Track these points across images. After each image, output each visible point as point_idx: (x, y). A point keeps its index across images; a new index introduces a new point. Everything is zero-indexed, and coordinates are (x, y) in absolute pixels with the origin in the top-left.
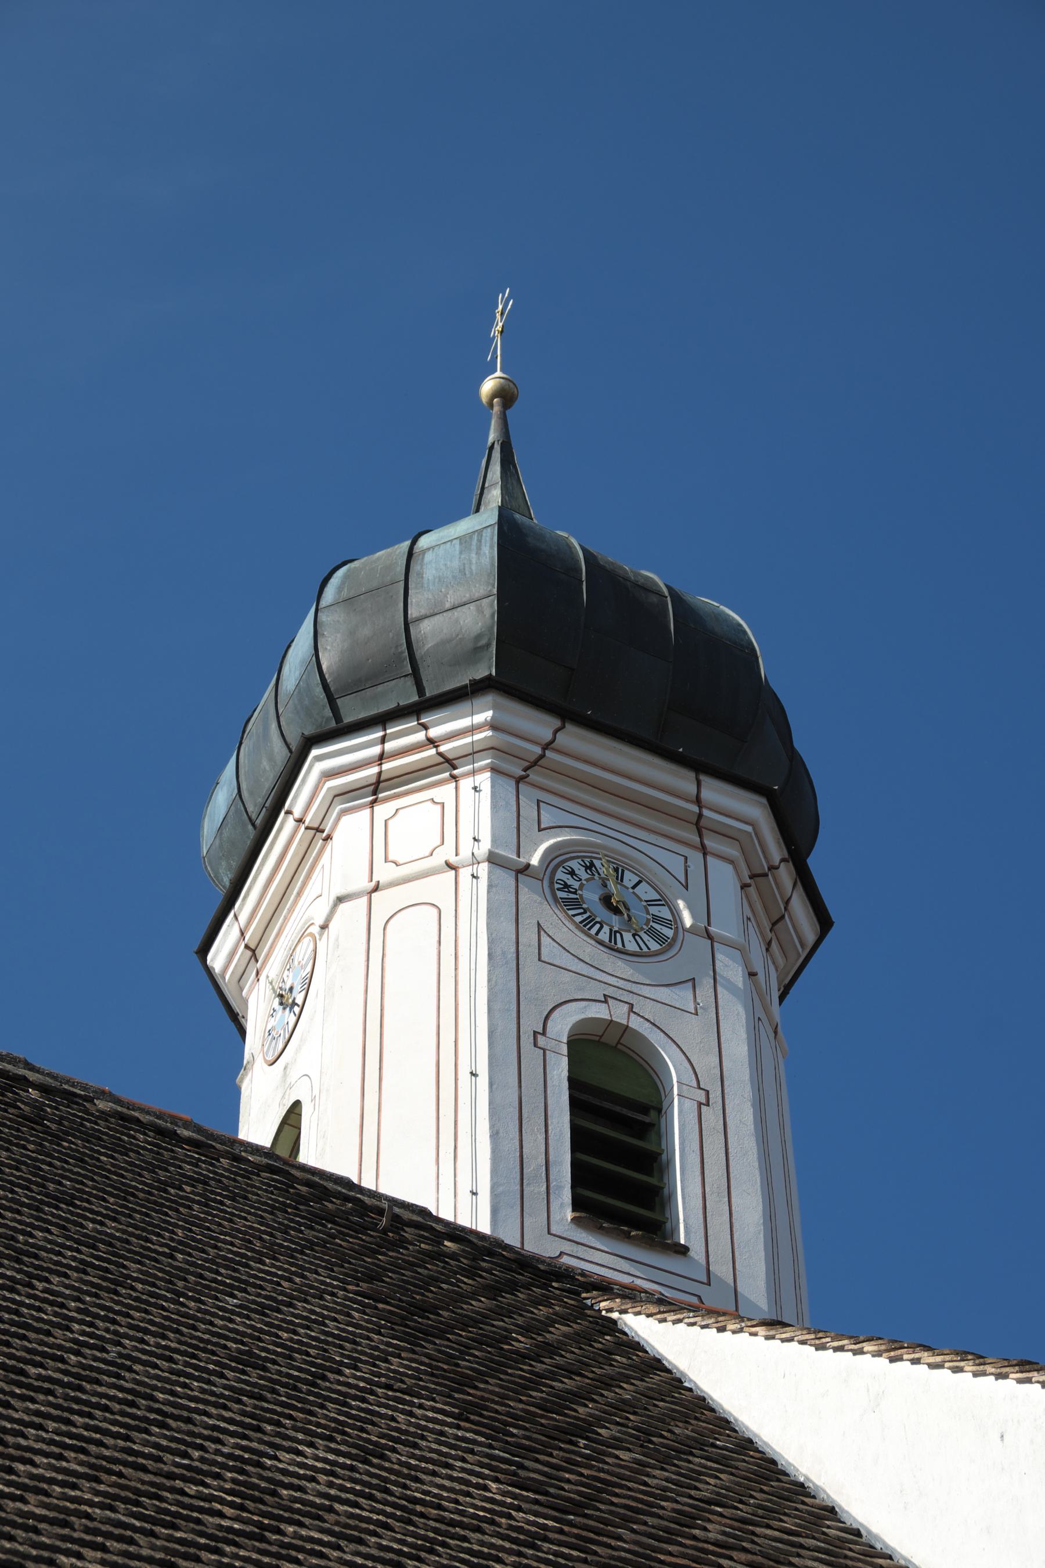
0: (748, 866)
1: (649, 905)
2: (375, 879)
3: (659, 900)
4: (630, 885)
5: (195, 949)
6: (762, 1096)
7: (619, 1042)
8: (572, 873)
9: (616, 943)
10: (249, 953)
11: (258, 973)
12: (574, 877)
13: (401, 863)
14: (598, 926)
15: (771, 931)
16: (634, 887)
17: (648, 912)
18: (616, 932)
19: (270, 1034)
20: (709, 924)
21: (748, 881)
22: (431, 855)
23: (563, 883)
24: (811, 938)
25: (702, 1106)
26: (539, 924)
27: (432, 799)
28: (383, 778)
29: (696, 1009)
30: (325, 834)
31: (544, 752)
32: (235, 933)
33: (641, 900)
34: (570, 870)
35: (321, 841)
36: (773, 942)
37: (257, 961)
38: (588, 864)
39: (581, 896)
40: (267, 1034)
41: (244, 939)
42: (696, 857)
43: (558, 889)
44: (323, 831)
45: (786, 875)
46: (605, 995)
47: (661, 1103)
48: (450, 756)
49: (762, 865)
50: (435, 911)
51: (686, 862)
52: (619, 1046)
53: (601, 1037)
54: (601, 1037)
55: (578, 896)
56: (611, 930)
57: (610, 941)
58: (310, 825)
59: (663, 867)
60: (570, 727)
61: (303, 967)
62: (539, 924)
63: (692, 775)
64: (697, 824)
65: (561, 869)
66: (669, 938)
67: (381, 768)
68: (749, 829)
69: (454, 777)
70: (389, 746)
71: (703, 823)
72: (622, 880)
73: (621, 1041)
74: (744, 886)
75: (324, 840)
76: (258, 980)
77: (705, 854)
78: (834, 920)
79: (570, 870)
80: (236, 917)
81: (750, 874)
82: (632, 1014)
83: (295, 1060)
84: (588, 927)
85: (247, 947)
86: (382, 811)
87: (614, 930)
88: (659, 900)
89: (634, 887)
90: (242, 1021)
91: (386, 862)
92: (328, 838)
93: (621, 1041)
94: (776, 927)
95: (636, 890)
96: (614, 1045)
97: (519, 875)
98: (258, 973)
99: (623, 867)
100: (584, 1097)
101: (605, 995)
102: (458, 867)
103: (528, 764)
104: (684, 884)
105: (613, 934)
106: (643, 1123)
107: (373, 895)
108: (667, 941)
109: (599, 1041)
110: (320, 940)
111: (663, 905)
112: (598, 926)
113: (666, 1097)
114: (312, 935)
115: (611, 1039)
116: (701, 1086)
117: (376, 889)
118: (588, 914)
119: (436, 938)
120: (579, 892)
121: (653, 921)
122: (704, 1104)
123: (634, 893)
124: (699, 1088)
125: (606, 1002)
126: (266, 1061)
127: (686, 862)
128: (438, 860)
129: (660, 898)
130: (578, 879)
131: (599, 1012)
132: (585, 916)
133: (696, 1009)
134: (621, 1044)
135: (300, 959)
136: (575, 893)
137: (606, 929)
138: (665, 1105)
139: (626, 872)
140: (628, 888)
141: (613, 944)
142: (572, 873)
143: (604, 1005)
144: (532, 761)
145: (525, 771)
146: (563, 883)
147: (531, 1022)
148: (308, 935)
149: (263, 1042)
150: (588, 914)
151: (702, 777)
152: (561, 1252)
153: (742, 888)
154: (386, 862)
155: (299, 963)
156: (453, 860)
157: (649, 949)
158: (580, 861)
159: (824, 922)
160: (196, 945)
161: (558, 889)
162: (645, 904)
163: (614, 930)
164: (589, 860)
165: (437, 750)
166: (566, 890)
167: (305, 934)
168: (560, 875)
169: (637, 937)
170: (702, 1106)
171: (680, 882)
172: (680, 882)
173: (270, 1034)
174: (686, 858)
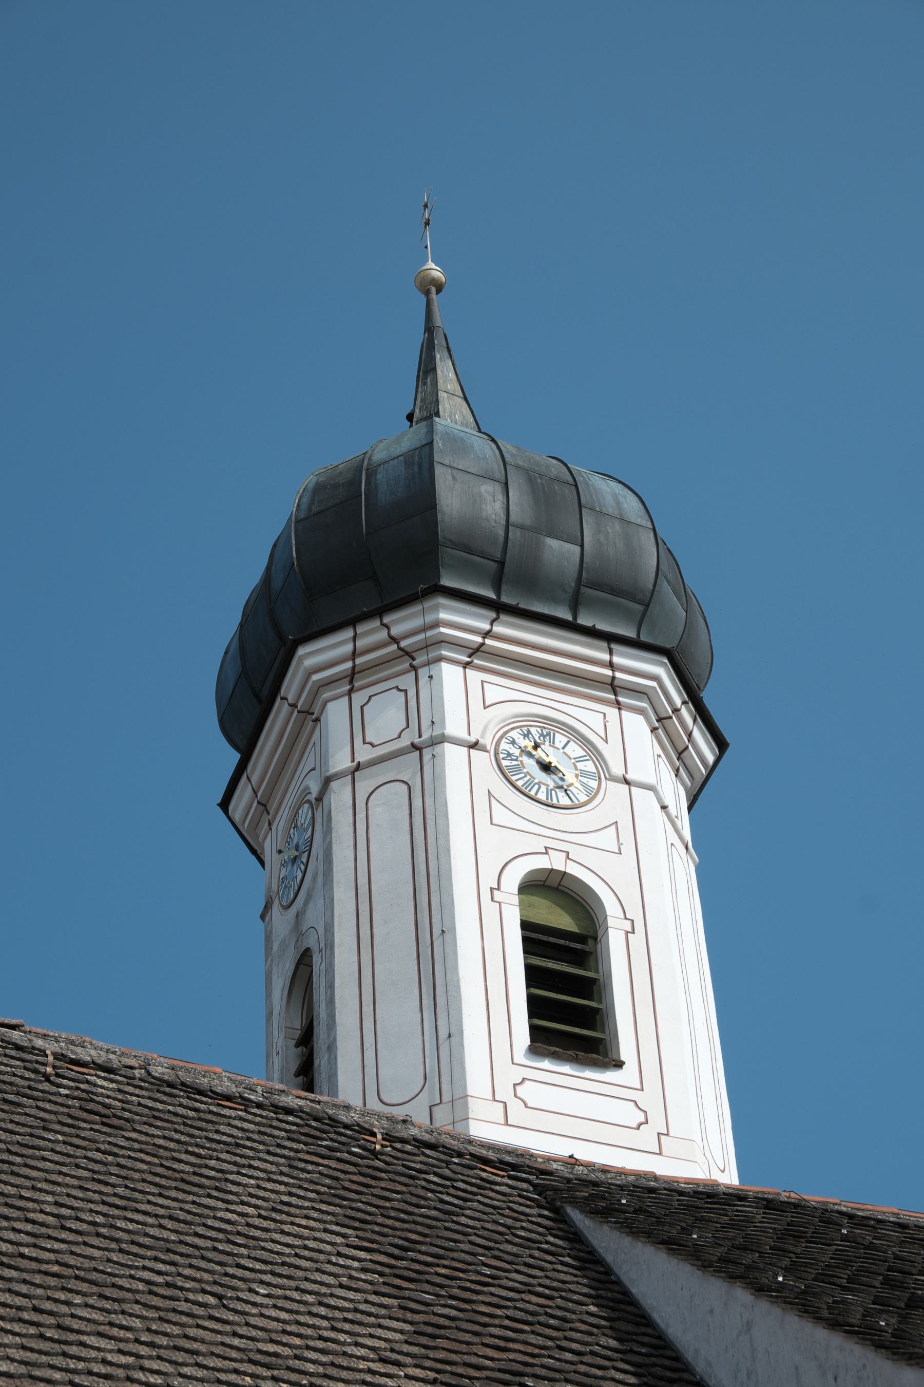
0: (656, 712)
1: (577, 762)
2: (356, 761)
3: (585, 756)
4: (560, 746)
5: (219, 801)
6: (677, 914)
7: (559, 884)
8: (513, 742)
9: (552, 800)
10: (262, 808)
11: (270, 824)
12: (515, 745)
13: (376, 744)
14: (537, 786)
15: (678, 759)
16: (563, 748)
17: (576, 769)
18: (551, 790)
19: (283, 882)
20: (626, 773)
21: (657, 725)
22: (399, 736)
23: (506, 752)
24: (711, 759)
25: (629, 934)
26: (489, 792)
27: (397, 687)
28: (357, 669)
29: (620, 849)
30: (314, 717)
31: (484, 641)
32: (249, 792)
33: (570, 758)
34: (511, 740)
35: (311, 722)
36: (681, 768)
37: (269, 814)
38: (526, 732)
39: (521, 762)
40: (281, 882)
41: (257, 796)
42: (612, 712)
43: (503, 759)
44: (313, 714)
45: (686, 714)
46: (546, 848)
47: (596, 932)
48: (409, 650)
49: (667, 711)
50: (405, 787)
51: (605, 718)
52: (560, 887)
53: (545, 881)
54: (545, 881)
55: (519, 763)
56: (547, 789)
57: (547, 799)
58: (301, 710)
59: (581, 833)
60: (503, 617)
61: (306, 830)
62: (489, 792)
63: (605, 645)
64: (612, 684)
65: (504, 740)
66: (594, 789)
67: (354, 663)
68: (653, 684)
69: (414, 668)
70: (361, 643)
71: (616, 683)
72: (554, 743)
73: (561, 884)
74: (654, 730)
75: (313, 721)
76: (271, 829)
77: (620, 709)
78: (728, 742)
79: (511, 740)
80: (249, 779)
81: (657, 718)
82: (568, 861)
83: (304, 911)
84: (528, 789)
85: (259, 803)
86: (359, 698)
87: (549, 788)
88: (585, 756)
89: (563, 748)
90: (262, 856)
91: (364, 744)
92: (317, 720)
93: (561, 884)
94: (682, 756)
95: (566, 750)
96: (556, 886)
97: (471, 750)
98: (270, 824)
99: (554, 730)
100: (534, 935)
101: (546, 848)
102: (422, 748)
103: (472, 651)
104: (604, 738)
105: (549, 792)
106: (583, 951)
107: (356, 773)
108: (591, 794)
109: (543, 885)
110: (317, 810)
111: (588, 760)
112: (537, 786)
113: (600, 927)
114: (309, 802)
115: (553, 882)
116: (628, 917)
117: (358, 767)
118: (528, 777)
119: (408, 812)
120: (520, 759)
121: (581, 776)
122: (630, 933)
123: (564, 753)
124: (626, 918)
125: (547, 853)
126: (282, 905)
127: (605, 718)
128: (405, 742)
129: (585, 754)
130: (518, 747)
131: (542, 863)
132: (526, 779)
133: (620, 849)
134: (562, 885)
135: (303, 822)
136: (516, 760)
137: (543, 788)
138: (600, 934)
139: (557, 734)
140: (558, 749)
141: (549, 801)
142: (513, 742)
143: (547, 856)
144: (475, 648)
145: (470, 658)
146: (506, 752)
147: (488, 881)
148: (305, 803)
149: (279, 887)
150: (528, 777)
151: (613, 646)
152: (523, 1078)
153: (652, 732)
154: (364, 744)
155: (302, 825)
156: (417, 741)
157: (579, 801)
158: (518, 730)
159: (721, 743)
160: (219, 797)
161: (503, 759)
162: (573, 761)
163: (549, 788)
164: (526, 728)
165: (398, 646)
166: (509, 758)
167: (305, 800)
168: (504, 746)
169: (568, 792)
170: (629, 934)
171: (601, 737)
172: (601, 737)
173: (283, 882)
174: (605, 715)
